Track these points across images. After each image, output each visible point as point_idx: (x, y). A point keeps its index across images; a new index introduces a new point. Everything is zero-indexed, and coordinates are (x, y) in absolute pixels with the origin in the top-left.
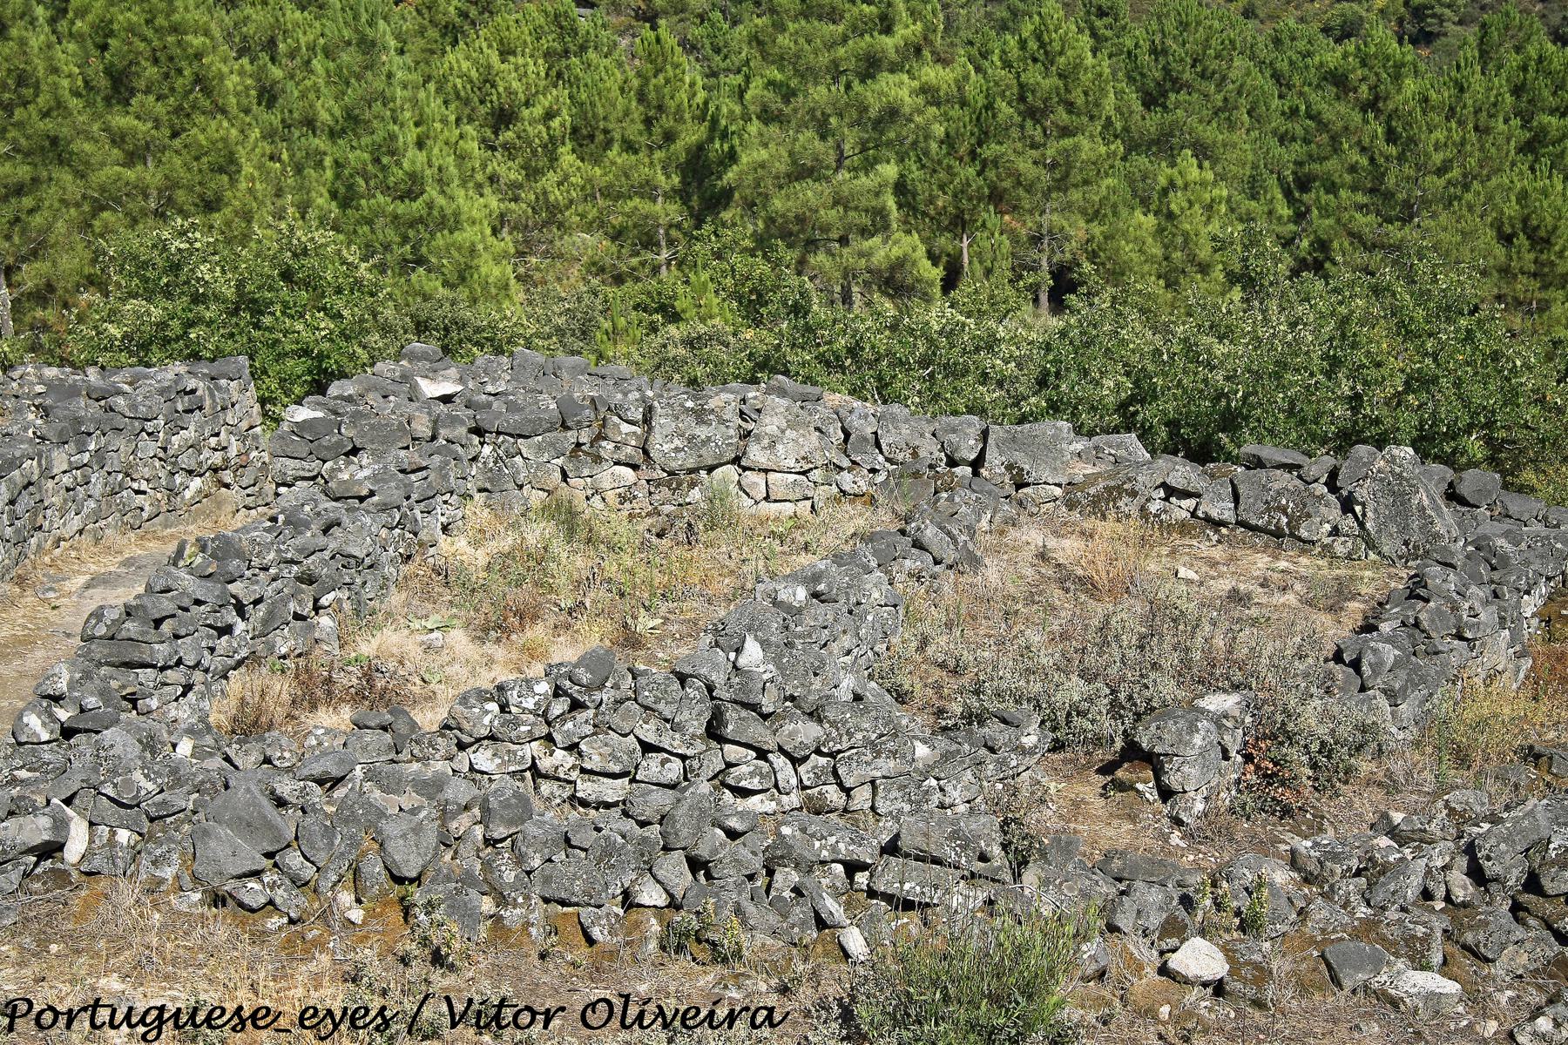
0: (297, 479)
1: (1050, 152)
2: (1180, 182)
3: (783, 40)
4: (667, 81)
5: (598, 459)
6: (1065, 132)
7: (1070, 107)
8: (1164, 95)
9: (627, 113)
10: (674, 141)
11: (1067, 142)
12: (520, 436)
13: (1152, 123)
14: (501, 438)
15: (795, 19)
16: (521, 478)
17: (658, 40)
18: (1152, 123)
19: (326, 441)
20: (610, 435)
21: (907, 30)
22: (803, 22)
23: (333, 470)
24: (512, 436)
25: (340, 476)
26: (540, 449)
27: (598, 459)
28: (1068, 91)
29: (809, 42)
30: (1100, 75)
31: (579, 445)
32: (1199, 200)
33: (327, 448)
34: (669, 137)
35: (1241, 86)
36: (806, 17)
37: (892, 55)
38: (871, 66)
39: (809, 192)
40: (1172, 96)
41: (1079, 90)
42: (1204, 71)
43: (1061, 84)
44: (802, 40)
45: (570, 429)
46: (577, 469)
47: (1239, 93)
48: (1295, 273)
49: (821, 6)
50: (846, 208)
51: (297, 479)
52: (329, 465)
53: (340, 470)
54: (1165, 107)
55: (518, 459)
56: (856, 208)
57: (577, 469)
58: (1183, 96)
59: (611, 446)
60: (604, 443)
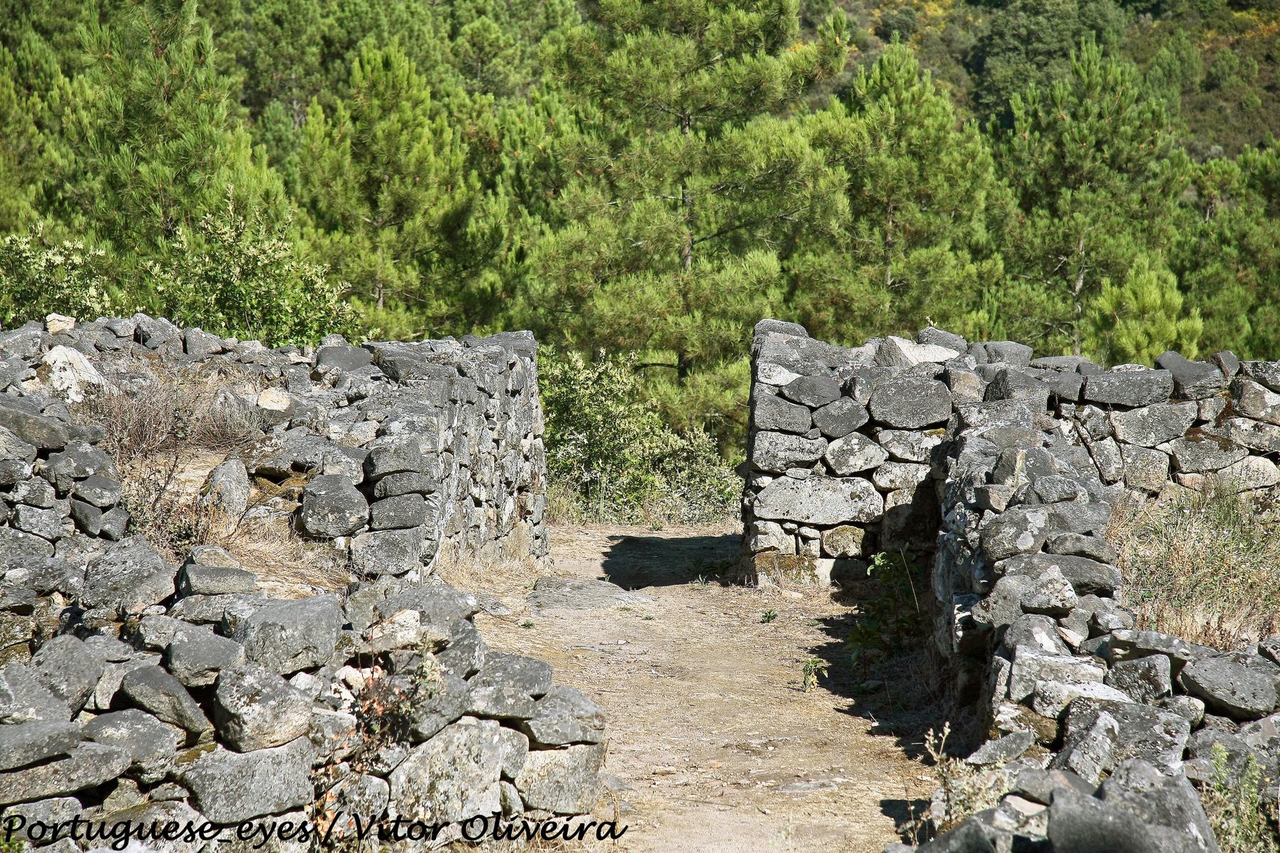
0: (788, 465)
1: (896, 267)
2: (1132, 305)
3: (618, 59)
4: (405, 125)
5: (1227, 445)
6: (919, 238)
7: (924, 199)
8: (1053, 193)
9: (337, 170)
10: (411, 215)
11: (920, 254)
12: (1118, 407)
13: (1037, 230)
14: (1087, 410)
15: (636, 30)
16: (1111, 472)
17: (387, 64)
18: (1037, 230)
19: (834, 409)
20: (1250, 409)
21: (800, 50)
22: (647, 33)
23: (843, 452)
24: (1104, 406)
25: (852, 461)
26: (1144, 426)
27: (1227, 445)
28: (923, 178)
29: (656, 62)
30: (973, 156)
31: (1198, 422)
32: (1161, 334)
33: (836, 419)
34: (403, 209)
35: (1168, 181)
36: (654, 28)
37: (780, 90)
38: (753, 99)
39: (651, 291)
40: (1067, 193)
41: (941, 177)
42: (1114, 158)
43: (914, 165)
44: (647, 61)
45: (1185, 398)
46: (1196, 459)
47: (1165, 193)
48: (232, 746)
49: (677, 12)
50: (707, 313)
51: (788, 465)
52: (836, 444)
53: (852, 452)
54: (1054, 212)
55: (1109, 442)
56: (723, 314)
57: (1196, 459)
58: (1083, 193)
59: (1247, 425)
60: (1238, 421)
